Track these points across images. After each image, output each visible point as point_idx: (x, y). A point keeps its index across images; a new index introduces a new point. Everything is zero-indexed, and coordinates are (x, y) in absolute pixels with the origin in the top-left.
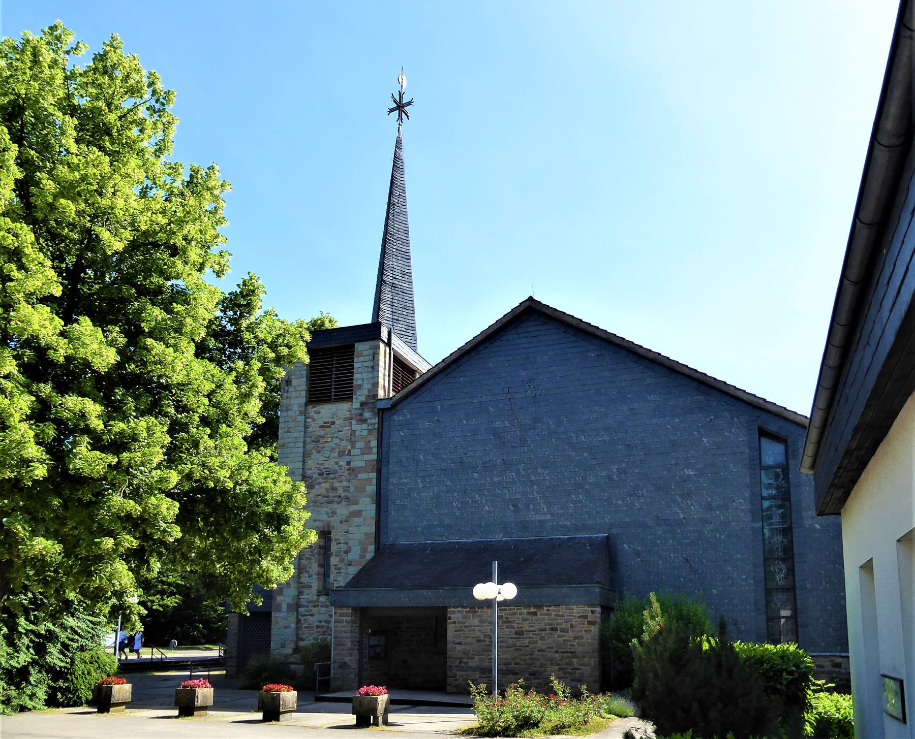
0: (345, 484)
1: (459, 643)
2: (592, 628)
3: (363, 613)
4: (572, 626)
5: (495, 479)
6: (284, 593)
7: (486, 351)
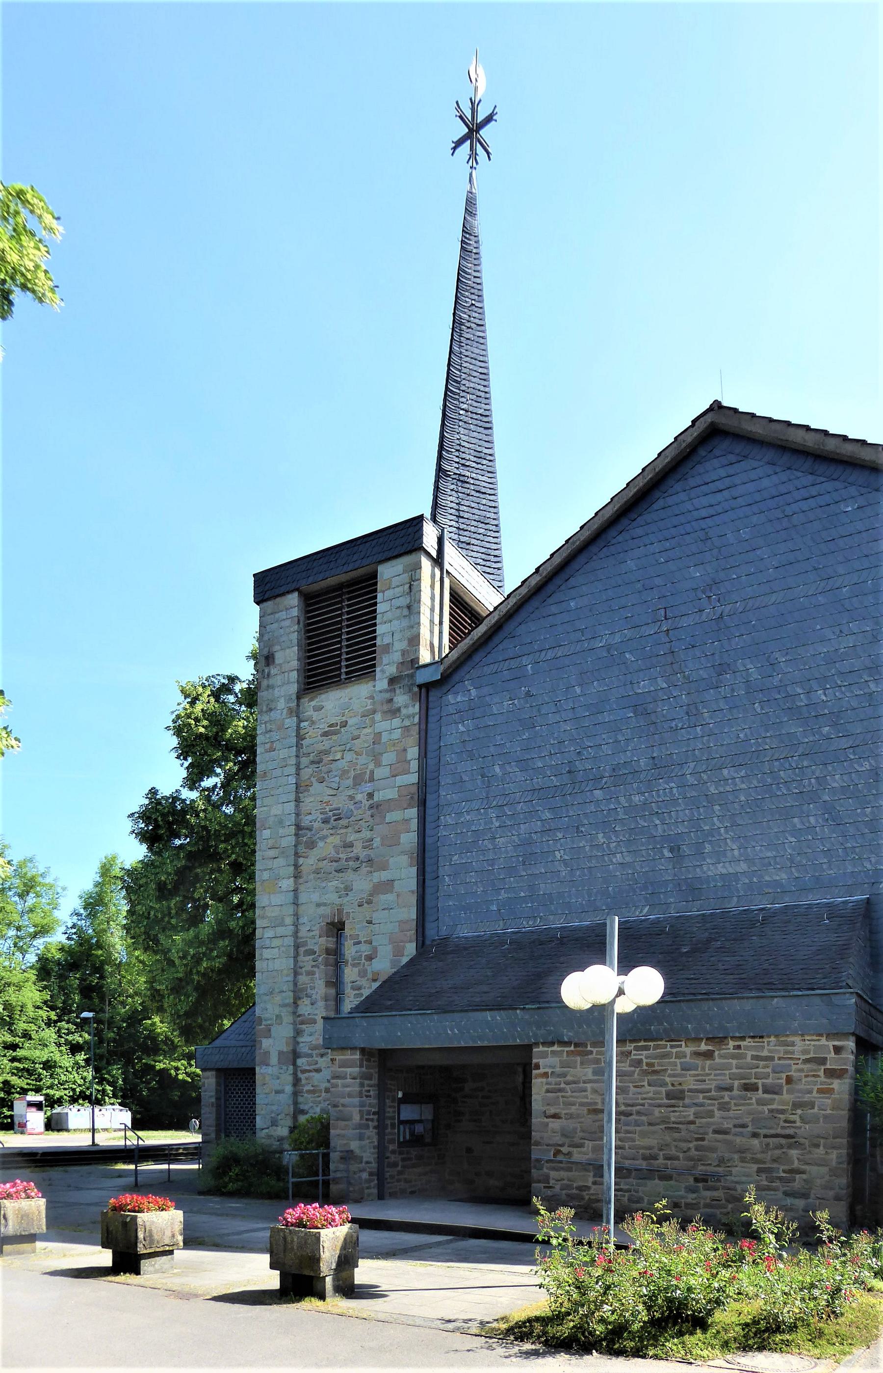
0: (366, 834)
1: (555, 1116)
2: (836, 1084)
3: (384, 1062)
4: (789, 1080)
5: (636, 799)
7: (620, 538)
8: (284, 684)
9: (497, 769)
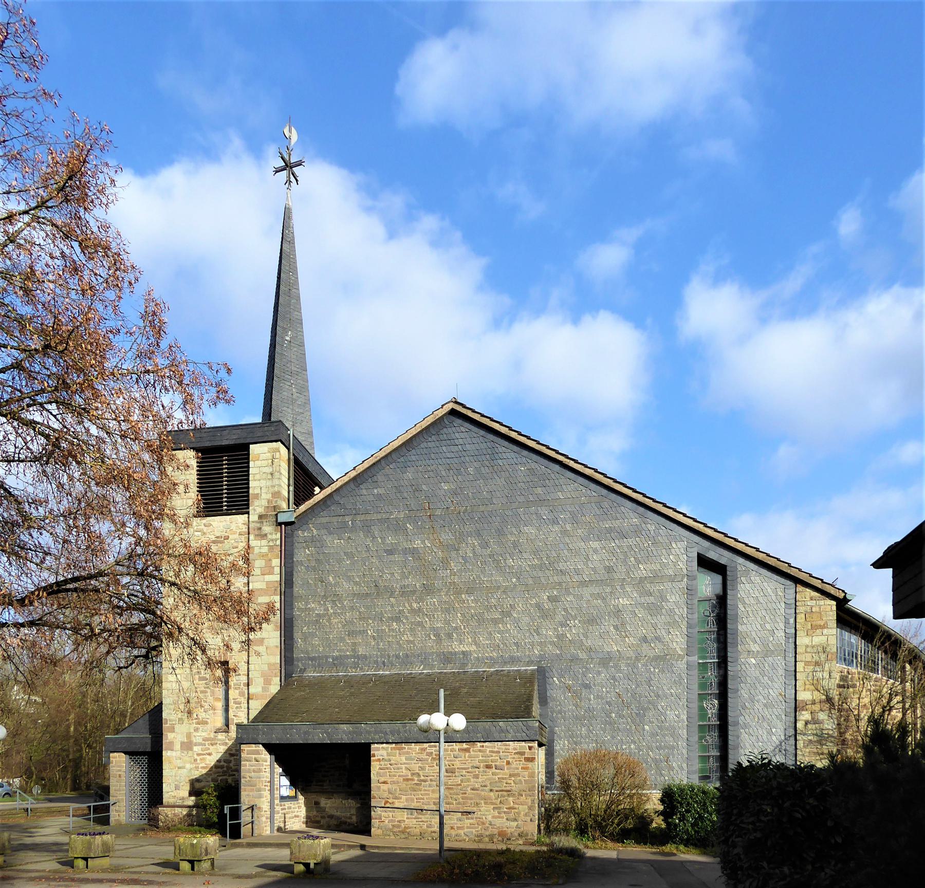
1: (385, 783)
4: (508, 763)
6: (176, 730)
8: (14, 428)
9: (331, 578)
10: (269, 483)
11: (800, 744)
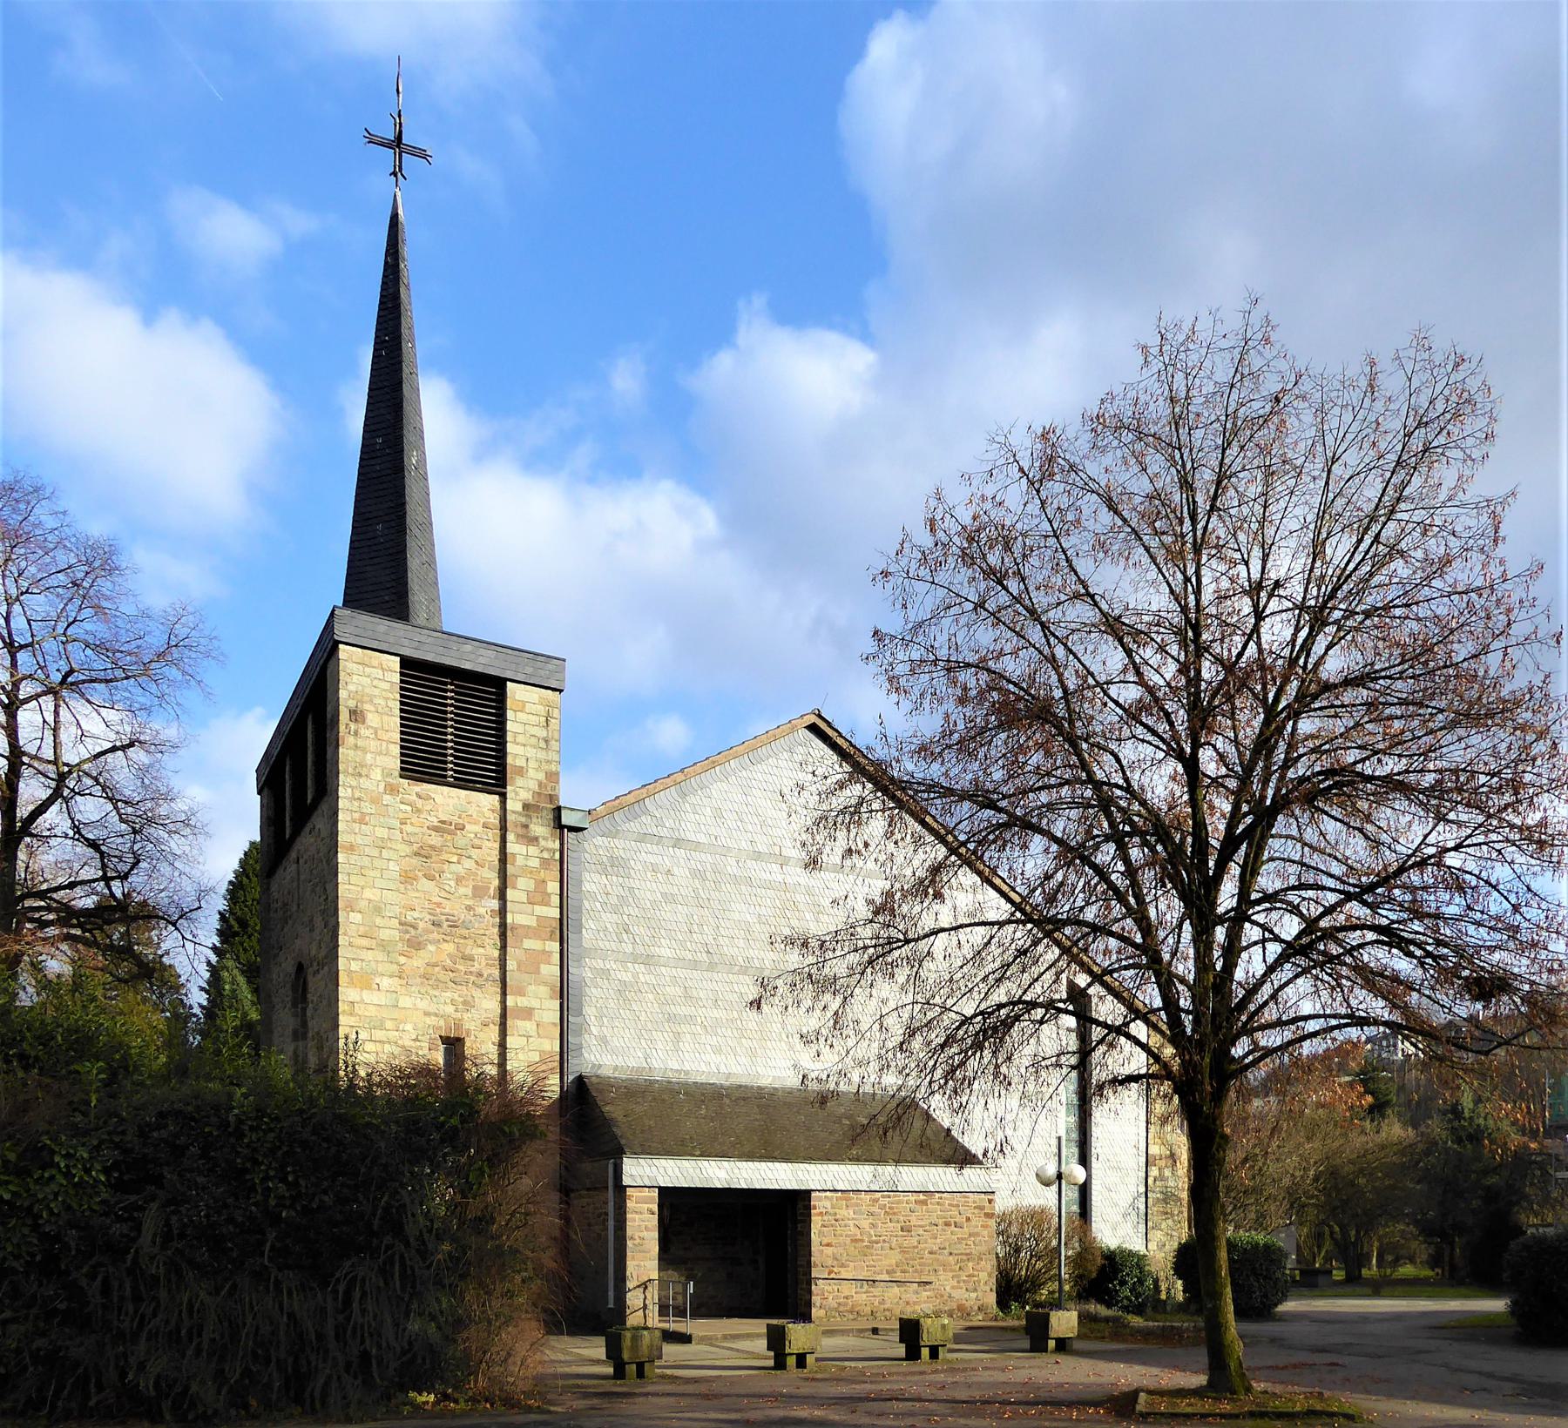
1: (828, 1245)
4: (968, 1219)
10: (542, 755)
11: (1150, 1201)
